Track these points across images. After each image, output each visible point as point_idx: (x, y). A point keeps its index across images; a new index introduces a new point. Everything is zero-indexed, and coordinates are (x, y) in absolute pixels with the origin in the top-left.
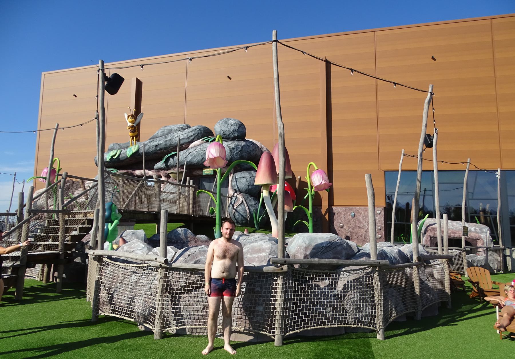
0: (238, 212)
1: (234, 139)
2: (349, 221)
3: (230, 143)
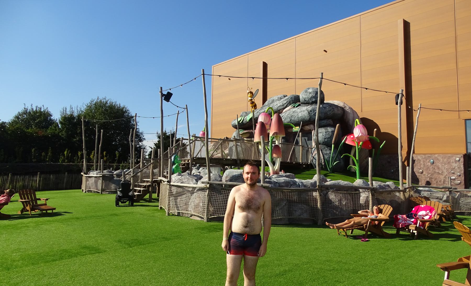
3: (309, 107)
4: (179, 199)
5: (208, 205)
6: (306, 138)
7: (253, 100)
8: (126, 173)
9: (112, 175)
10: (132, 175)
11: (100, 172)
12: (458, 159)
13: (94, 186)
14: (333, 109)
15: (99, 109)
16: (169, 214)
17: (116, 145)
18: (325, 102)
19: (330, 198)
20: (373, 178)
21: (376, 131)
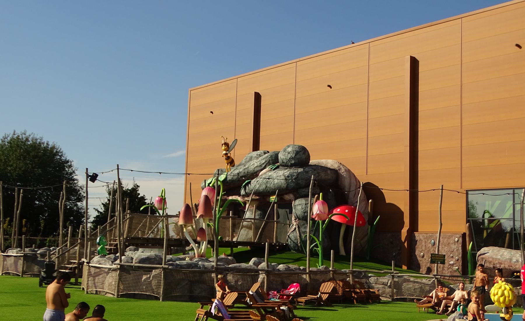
0: (290, 239)
1: (292, 166)
2: (429, 250)
3: (287, 171)
4: (97, 279)
5: (119, 283)
6: (288, 210)
7: (229, 155)
8: (52, 253)
9: (35, 255)
10: (57, 256)
11: (21, 251)
12: (457, 239)
13: (13, 267)
14: (318, 173)
15: (16, 151)
16: (87, 293)
17: (40, 206)
18: (312, 162)
19: (228, 279)
21: (371, 202)
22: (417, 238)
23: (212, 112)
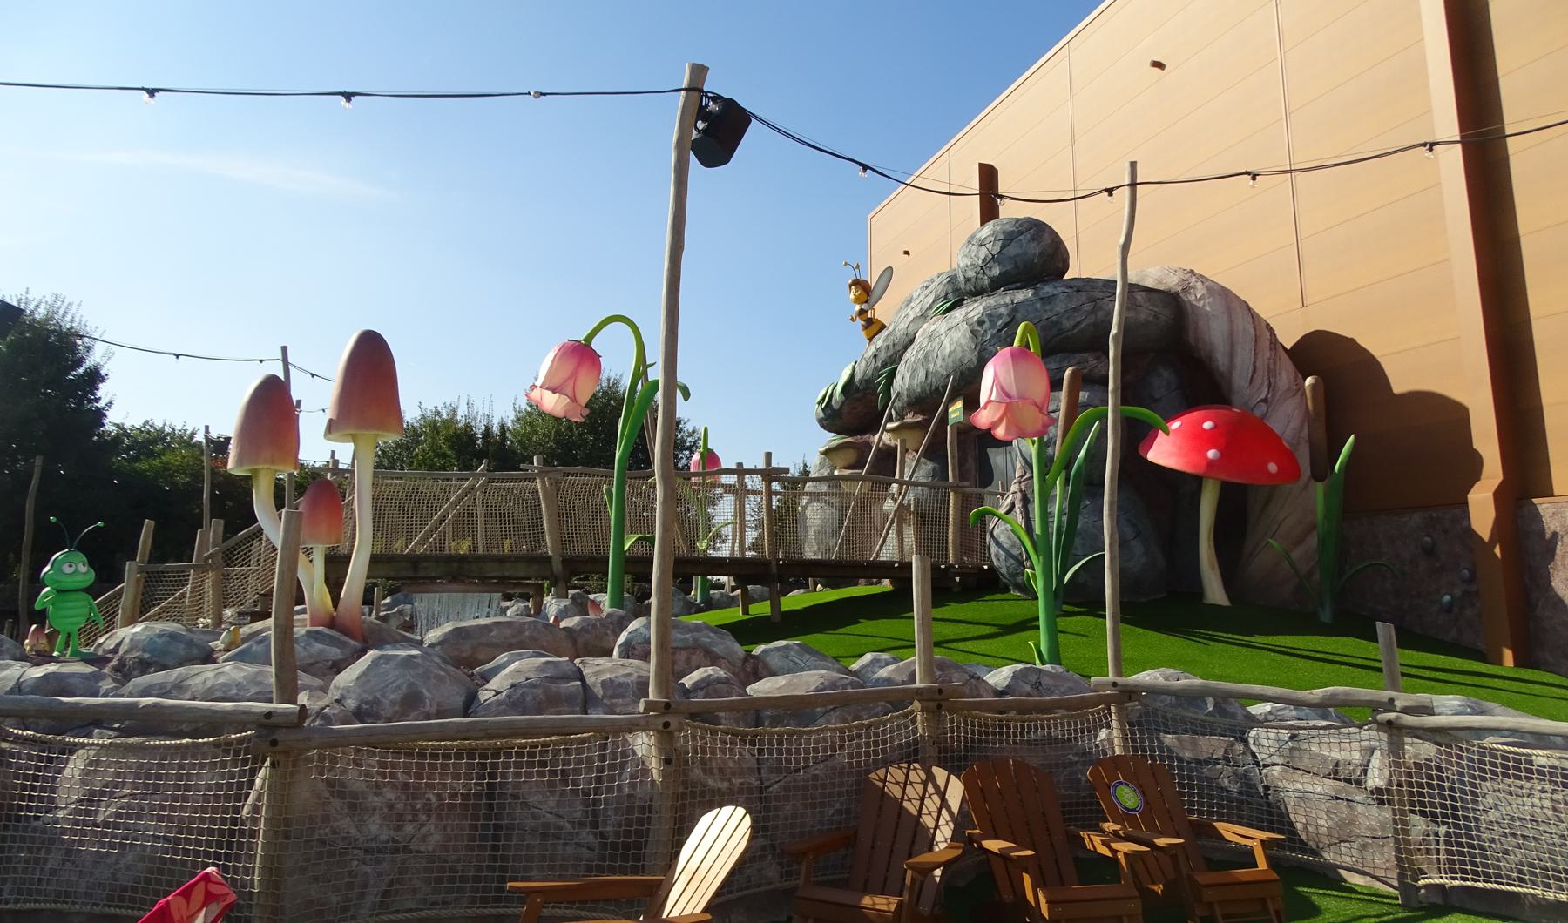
0: (997, 543)
14: (1095, 300)
20: (1062, 623)
21: (1314, 386)
22: (1551, 524)
23: (907, 253)
